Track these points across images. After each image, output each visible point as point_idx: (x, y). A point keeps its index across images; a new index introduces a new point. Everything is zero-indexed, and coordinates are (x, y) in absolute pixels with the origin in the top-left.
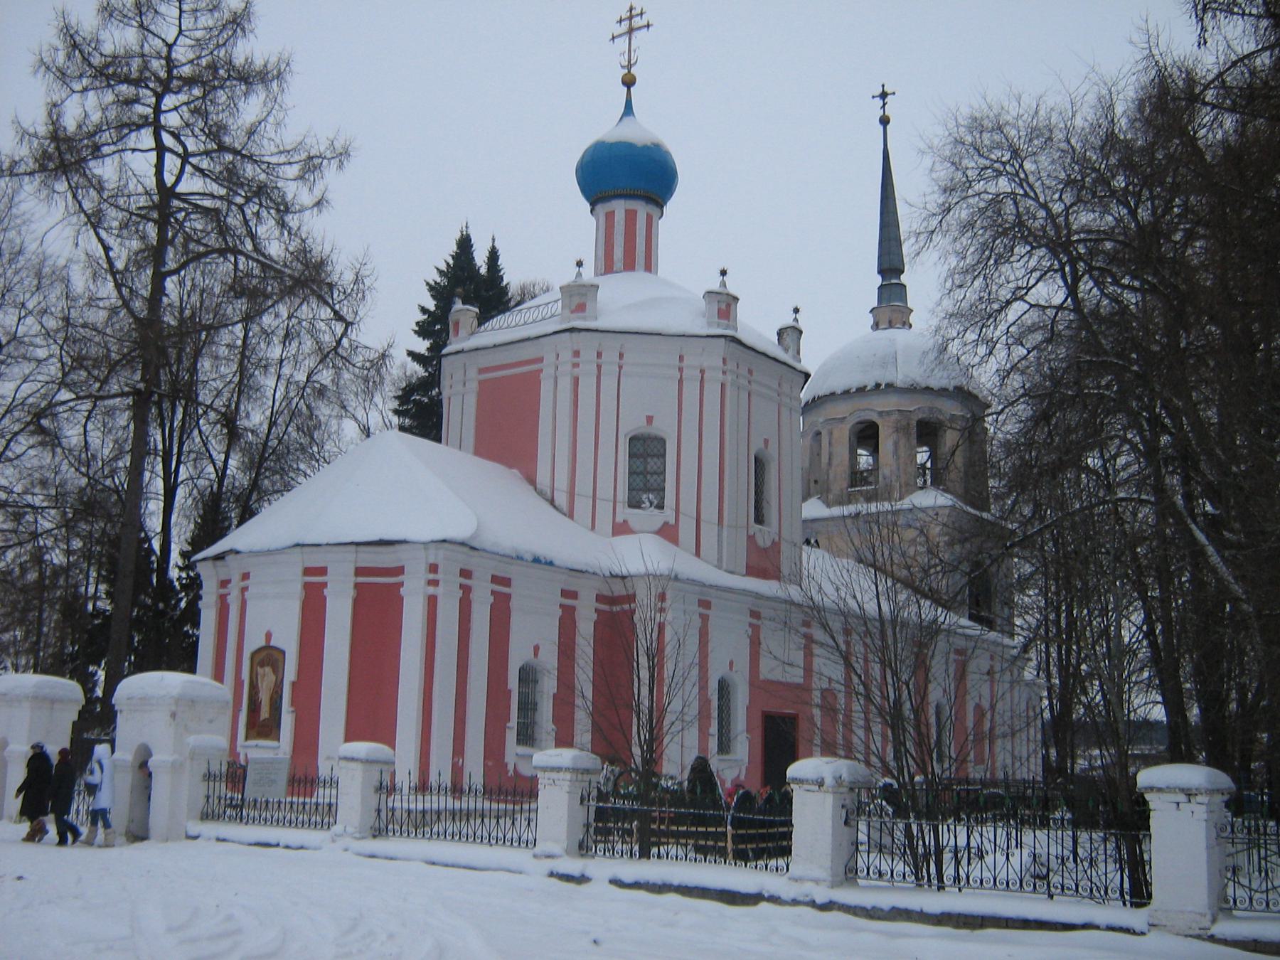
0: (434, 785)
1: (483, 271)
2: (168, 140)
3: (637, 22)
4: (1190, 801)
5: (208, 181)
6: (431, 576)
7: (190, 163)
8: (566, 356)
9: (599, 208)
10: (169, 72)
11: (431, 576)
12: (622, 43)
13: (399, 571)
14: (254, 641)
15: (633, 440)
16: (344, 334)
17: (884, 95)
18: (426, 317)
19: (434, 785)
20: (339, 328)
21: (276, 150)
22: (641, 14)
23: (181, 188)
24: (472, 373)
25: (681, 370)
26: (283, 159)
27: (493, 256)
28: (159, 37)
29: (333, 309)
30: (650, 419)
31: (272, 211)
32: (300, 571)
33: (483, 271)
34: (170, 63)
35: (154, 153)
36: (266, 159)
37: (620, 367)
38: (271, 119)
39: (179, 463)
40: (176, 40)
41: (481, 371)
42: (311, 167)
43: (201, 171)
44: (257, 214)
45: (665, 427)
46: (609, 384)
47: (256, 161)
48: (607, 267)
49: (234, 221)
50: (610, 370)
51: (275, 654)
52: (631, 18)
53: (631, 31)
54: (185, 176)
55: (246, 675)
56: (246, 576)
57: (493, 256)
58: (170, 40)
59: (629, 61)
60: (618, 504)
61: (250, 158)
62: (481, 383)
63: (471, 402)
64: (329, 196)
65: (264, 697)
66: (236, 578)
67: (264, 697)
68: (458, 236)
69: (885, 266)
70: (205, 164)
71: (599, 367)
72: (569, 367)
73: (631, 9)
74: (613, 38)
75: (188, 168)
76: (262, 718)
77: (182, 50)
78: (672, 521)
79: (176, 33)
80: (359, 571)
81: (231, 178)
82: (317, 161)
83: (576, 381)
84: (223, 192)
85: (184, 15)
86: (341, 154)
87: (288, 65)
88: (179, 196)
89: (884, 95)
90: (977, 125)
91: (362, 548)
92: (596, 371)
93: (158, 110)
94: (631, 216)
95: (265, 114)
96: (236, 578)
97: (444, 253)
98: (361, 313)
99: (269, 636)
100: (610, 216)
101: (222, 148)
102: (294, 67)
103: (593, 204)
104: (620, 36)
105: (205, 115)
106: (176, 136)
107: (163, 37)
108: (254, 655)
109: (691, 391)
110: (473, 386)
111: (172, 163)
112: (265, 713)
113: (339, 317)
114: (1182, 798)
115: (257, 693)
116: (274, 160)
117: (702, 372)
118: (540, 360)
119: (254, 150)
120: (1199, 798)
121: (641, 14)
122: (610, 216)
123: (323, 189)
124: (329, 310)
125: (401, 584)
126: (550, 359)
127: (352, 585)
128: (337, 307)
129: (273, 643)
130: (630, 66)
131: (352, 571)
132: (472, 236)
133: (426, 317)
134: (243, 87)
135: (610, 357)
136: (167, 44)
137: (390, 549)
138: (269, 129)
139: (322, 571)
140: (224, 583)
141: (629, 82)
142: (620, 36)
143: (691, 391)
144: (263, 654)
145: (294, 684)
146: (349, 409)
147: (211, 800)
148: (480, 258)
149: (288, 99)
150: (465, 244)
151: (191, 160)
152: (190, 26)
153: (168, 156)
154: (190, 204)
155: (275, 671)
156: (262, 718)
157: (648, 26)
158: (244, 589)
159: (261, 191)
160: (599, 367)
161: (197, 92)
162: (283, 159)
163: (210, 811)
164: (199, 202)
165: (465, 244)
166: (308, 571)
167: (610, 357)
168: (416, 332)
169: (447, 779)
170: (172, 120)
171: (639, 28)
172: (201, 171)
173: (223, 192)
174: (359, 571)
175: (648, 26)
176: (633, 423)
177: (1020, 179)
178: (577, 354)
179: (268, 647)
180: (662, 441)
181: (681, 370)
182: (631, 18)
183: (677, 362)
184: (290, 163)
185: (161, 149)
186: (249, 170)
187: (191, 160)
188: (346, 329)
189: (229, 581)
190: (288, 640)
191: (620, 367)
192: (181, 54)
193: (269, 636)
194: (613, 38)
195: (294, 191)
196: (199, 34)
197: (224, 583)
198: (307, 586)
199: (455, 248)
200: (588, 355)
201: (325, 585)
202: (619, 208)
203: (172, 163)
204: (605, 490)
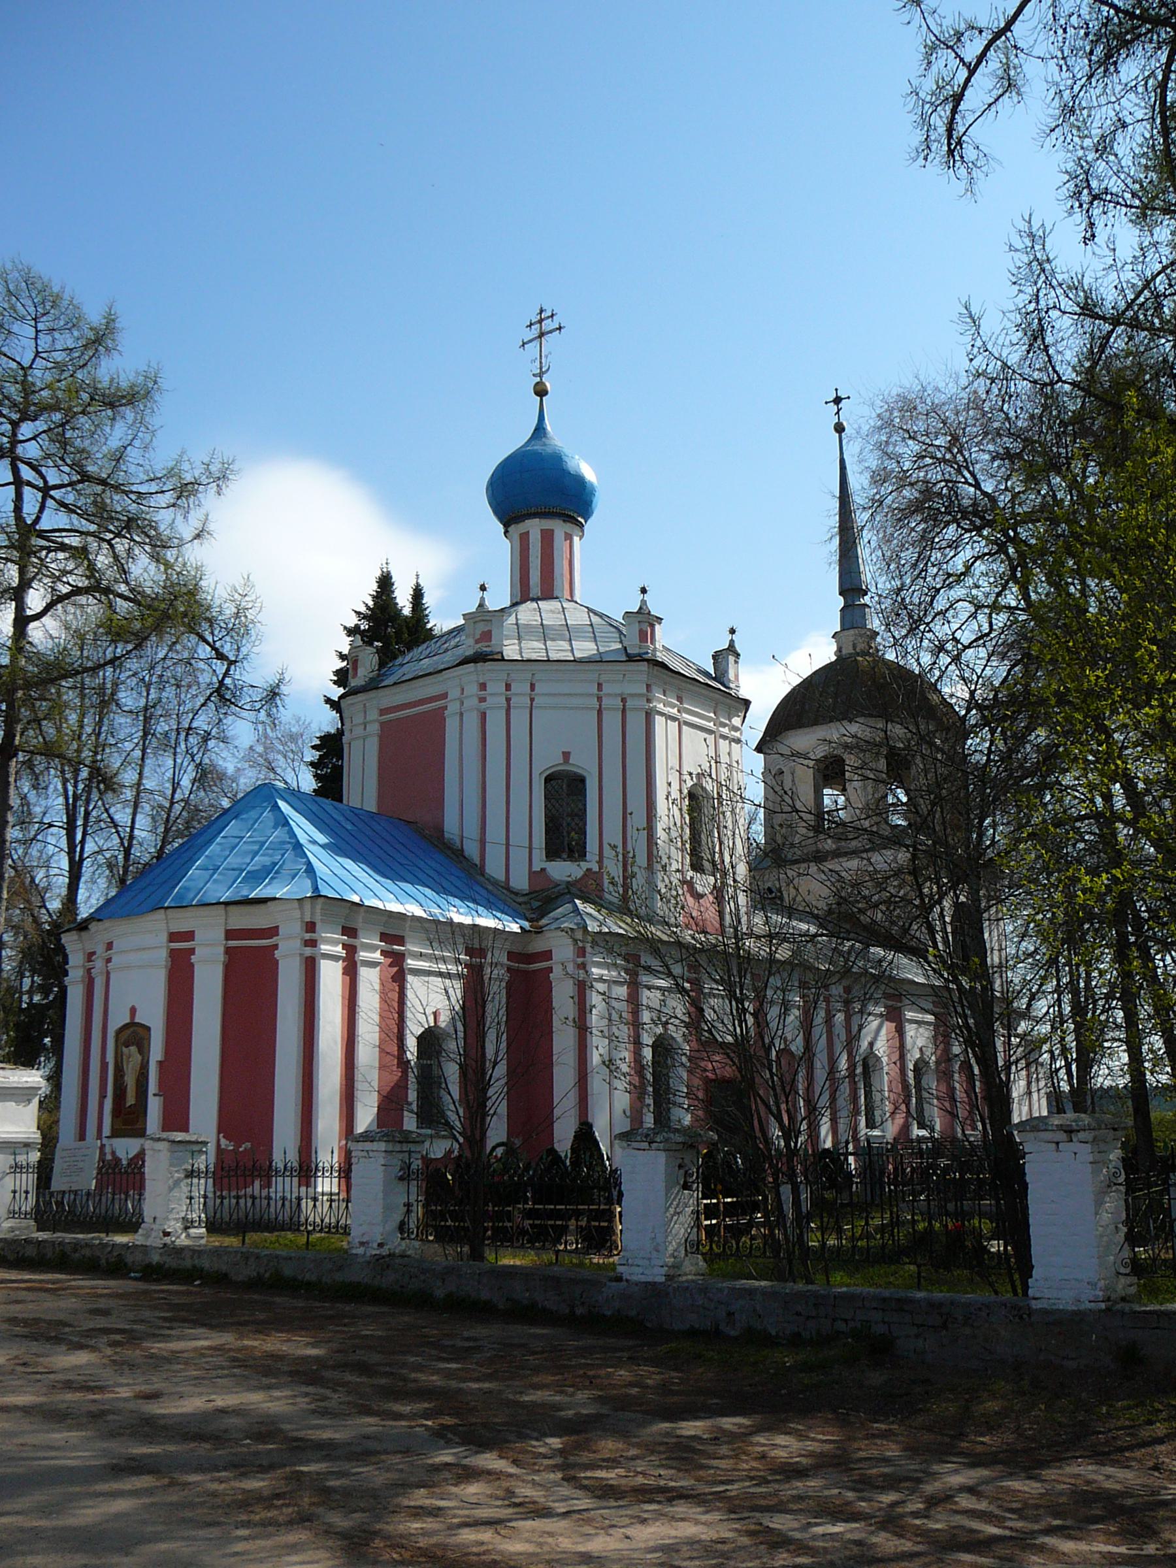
0: (281, 1166)
1: (407, 611)
2: (27, 473)
3: (548, 325)
4: (1071, 1141)
5: (74, 516)
6: (308, 936)
7: (52, 498)
8: (472, 689)
9: (511, 529)
10: (25, 398)
11: (308, 936)
12: (533, 348)
13: (273, 931)
14: (119, 1019)
15: (548, 780)
16: (226, 674)
17: (837, 400)
18: (345, 663)
19: (281, 1166)
20: (220, 667)
21: (146, 478)
22: (552, 316)
23: (44, 525)
24: (373, 715)
25: (599, 699)
26: (153, 487)
27: (418, 594)
28: (14, 360)
29: (213, 648)
30: (566, 755)
31: (147, 548)
32: (164, 937)
33: (407, 611)
34: (27, 389)
35: (13, 487)
36: (134, 488)
37: (532, 700)
38: (137, 443)
39: (85, 834)
40: (32, 363)
41: (383, 712)
42: (186, 491)
43: (62, 504)
44: (129, 551)
45: (584, 762)
46: (519, 719)
47: (124, 492)
48: (523, 594)
49: (103, 560)
50: (520, 701)
51: (140, 1030)
52: (541, 321)
53: (542, 335)
54: (46, 512)
55: (110, 1058)
56: (110, 946)
57: (418, 594)
58: (26, 364)
59: (541, 368)
60: (534, 851)
61: (117, 488)
62: (382, 724)
63: (373, 746)
64: (211, 527)
65: (130, 1080)
66: (100, 950)
67: (130, 1080)
68: (378, 574)
69: (848, 586)
70: (70, 499)
71: (508, 700)
72: (475, 701)
73: (542, 311)
74: (524, 344)
75: (50, 503)
76: (128, 1104)
77: (38, 373)
78: (596, 868)
79: (32, 356)
80: (230, 934)
81: (101, 513)
82: (189, 487)
83: (483, 716)
84: (93, 528)
85: (41, 335)
86: (219, 479)
87: (155, 382)
88: (41, 534)
89: (837, 400)
90: (908, 407)
91: (231, 908)
92: (505, 705)
93: (14, 442)
94: (548, 538)
95: (130, 437)
96: (100, 950)
97: (363, 595)
98: (244, 650)
99: (133, 1011)
100: (524, 538)
101: (86, 477)
102: (163, 383)
103: (506, 525)
104: (530, 341)
105: (64, 443)
106: (35, 468)
107: (18, 359)
108: (119, 1031)
109: (612, 721)
110: (374, 728)
111: (31, 498)
112: (131, 1100)
113: (220, 656)
114: (1062, 1136)
115: (122, 1076)
116: (143, 489)
117: (624, 700)
118: (444, 696)
119: (121, 477)
120: (1082, 1135)
121: (552, 316)
122: (524, 538)
123: (203, 518)
124: (208, 649)
125: (276, 947)
126: (454, 693)
127: (222, 949)
128: (218, 644)
129: (137, 1020)
130: (541, 375)
131: (223, 936)
132: (393, 574)
133: (345, 663)
134: (109, 412)
135: (520, 688)
136: (23, 368)
137: (262, 907)
138: (133, 454)
139: (189, 936)
140: (90, 956)
141: (541, 392)
142: (530, 341)
143: (612, 721)
144: (128, 1032)
145: (160, 1063)
146: (279, 771)
147: (17, 1195)
148: (403, 599)
149: (155, 421)
150: (385, 583)
151: (52, 493)
152: (47, 346)
153: (27, 490)
154: (53, 542)
155: (140, 1052)
156: (128, 1104)
157: (560, 328)
158: (109, 960)
159: (131, 524)
160: (508, 700)
161: (57, 417)
162: (153, 487)
163: (17, 1209)
164: (66, 541)
165: (385, 583)
166: (174, 937)
167: (520, 688)
168: (335, 683)
169: (293, 1157)
170: (31, 450)
171: (551, 332)
172: (62, 504)
173: (93, 528)
174: (230, 934)
175: (560, 328)
176: (548, 760)
177: (959, 466)
178: (483, 686)
179: (132, 1024)
180: (582, 780)
181: (599, 699)
182: (541, 321)
183: (596, 691)
184: (163, 492)
185: (18, 483)
186: (118, 502)
187: (52, 493)
188: (228, 670)
189: (94, 953)
190: (154, 1016)
191: (532, 700)
192: (38, 376)
193: (133, 1011)
194: (524, 344)
195: (164, 518)
196: (59, 356)
197: (90, 956)
198: (173, 953)
199: (375, 586)
200: (496, 687)
201: (192, 951)
202: (534, 527)
203: (31, 498)
204: (519, 836)
